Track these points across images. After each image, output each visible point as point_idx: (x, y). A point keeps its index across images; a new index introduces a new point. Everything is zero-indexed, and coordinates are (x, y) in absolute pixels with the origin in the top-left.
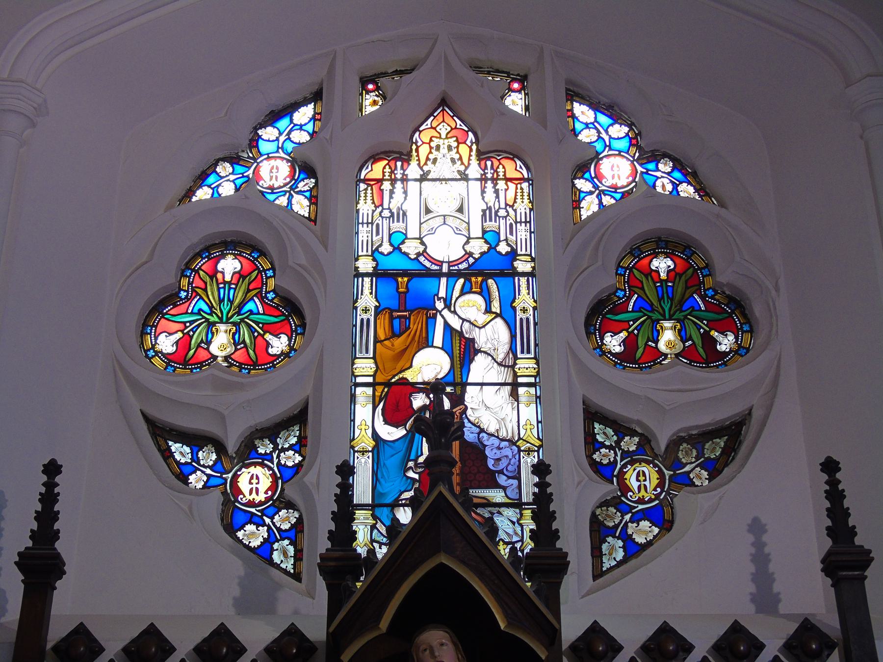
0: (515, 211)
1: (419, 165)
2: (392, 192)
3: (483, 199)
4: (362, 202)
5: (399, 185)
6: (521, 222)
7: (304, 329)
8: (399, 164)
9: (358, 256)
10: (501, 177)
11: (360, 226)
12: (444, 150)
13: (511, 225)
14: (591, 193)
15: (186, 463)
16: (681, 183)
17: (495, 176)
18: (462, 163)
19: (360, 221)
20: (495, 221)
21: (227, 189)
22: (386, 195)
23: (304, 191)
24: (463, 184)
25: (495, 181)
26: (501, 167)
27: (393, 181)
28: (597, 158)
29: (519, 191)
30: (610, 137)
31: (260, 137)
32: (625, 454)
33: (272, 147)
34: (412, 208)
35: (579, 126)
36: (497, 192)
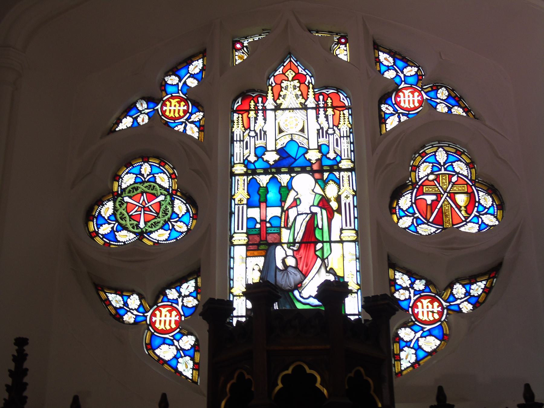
0: (339, 130)
1: (274, 99)
2: (256, 119)
3: (317, 121)
4: (235, 126)
5: (260, 113)
6: (343, 137)
7: (197, 216)
8: (260, 99)
9: (235, 164)
10: (330, 106)
11: (235, 143)
12: (290, 89)
13: (337, 139)
14: (392, 114)
15: (121, 308)
16: (453, 106)
17: (325, 105)
18: (303, 98)
19: (235, 139)
20: (326, 138)
21: (143, 119)
22: (252, 120)
23: (195, 122)
24: (304, 112)
25: (325, 108)
26: (329, 99)
27: (256, 110)
28: (398, 90)
29: (342, 115)
30: (405, 76)
31: (166, 83)
32: (416, 292)
33: (174, 89)
34: (270, 128)
35: (383, 69)
36: (327, 117)
